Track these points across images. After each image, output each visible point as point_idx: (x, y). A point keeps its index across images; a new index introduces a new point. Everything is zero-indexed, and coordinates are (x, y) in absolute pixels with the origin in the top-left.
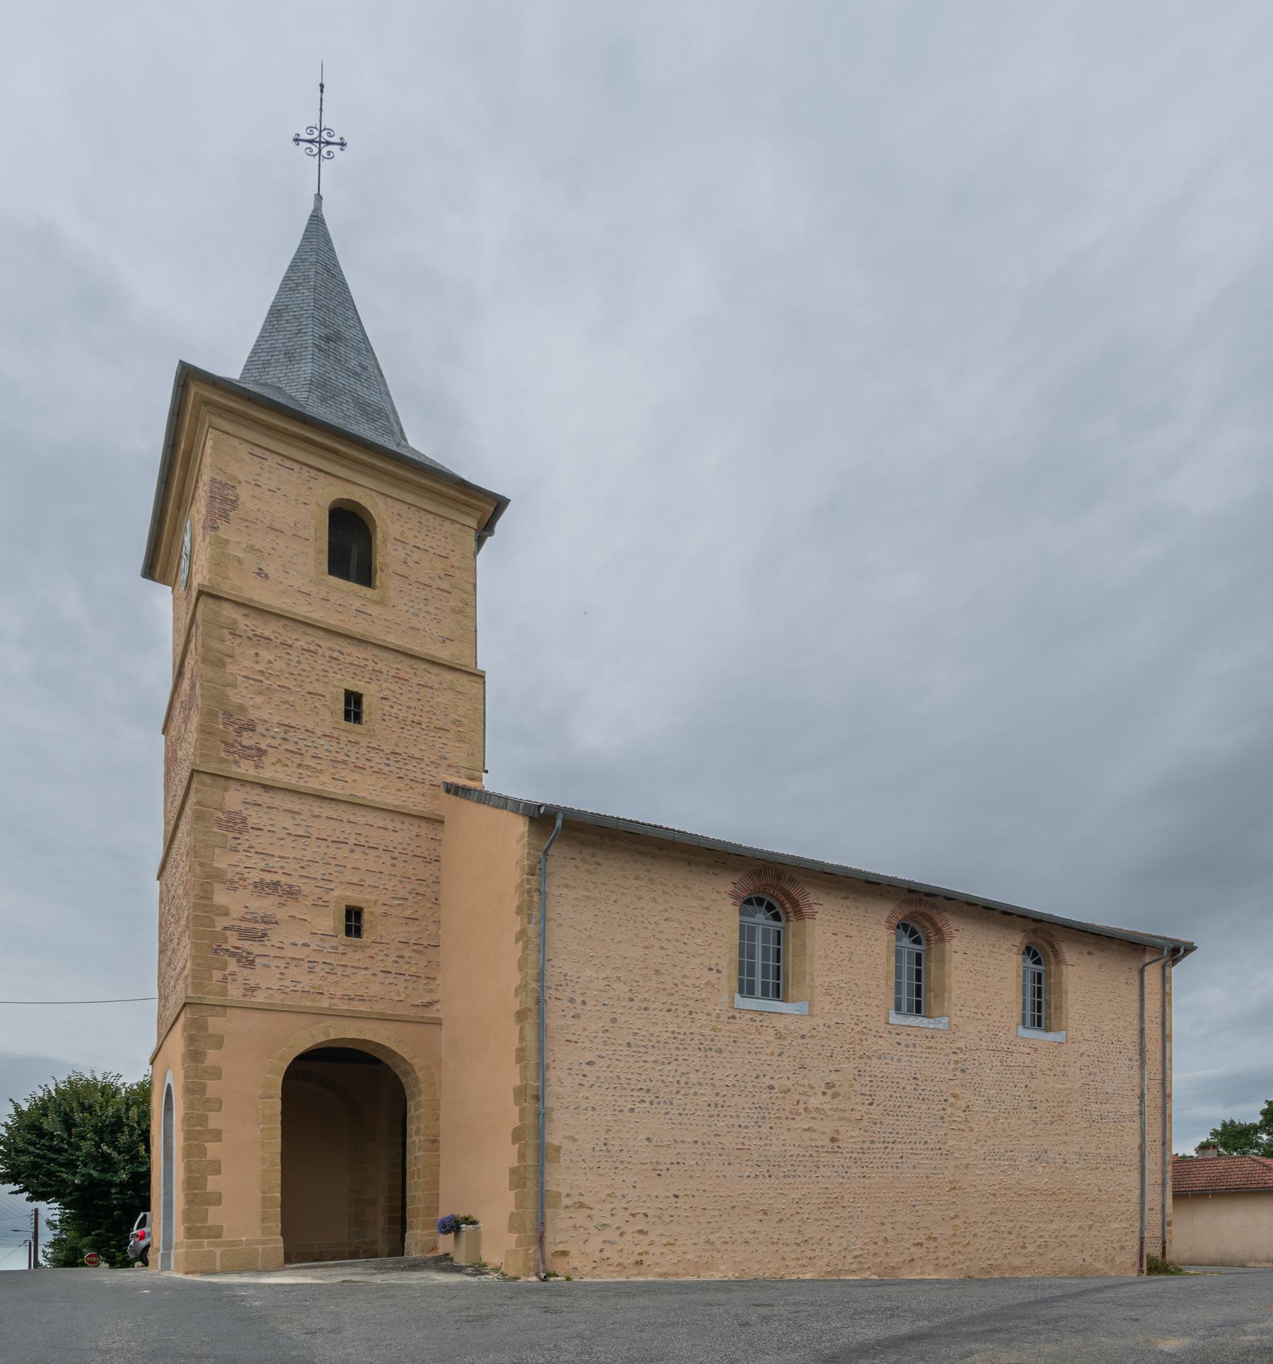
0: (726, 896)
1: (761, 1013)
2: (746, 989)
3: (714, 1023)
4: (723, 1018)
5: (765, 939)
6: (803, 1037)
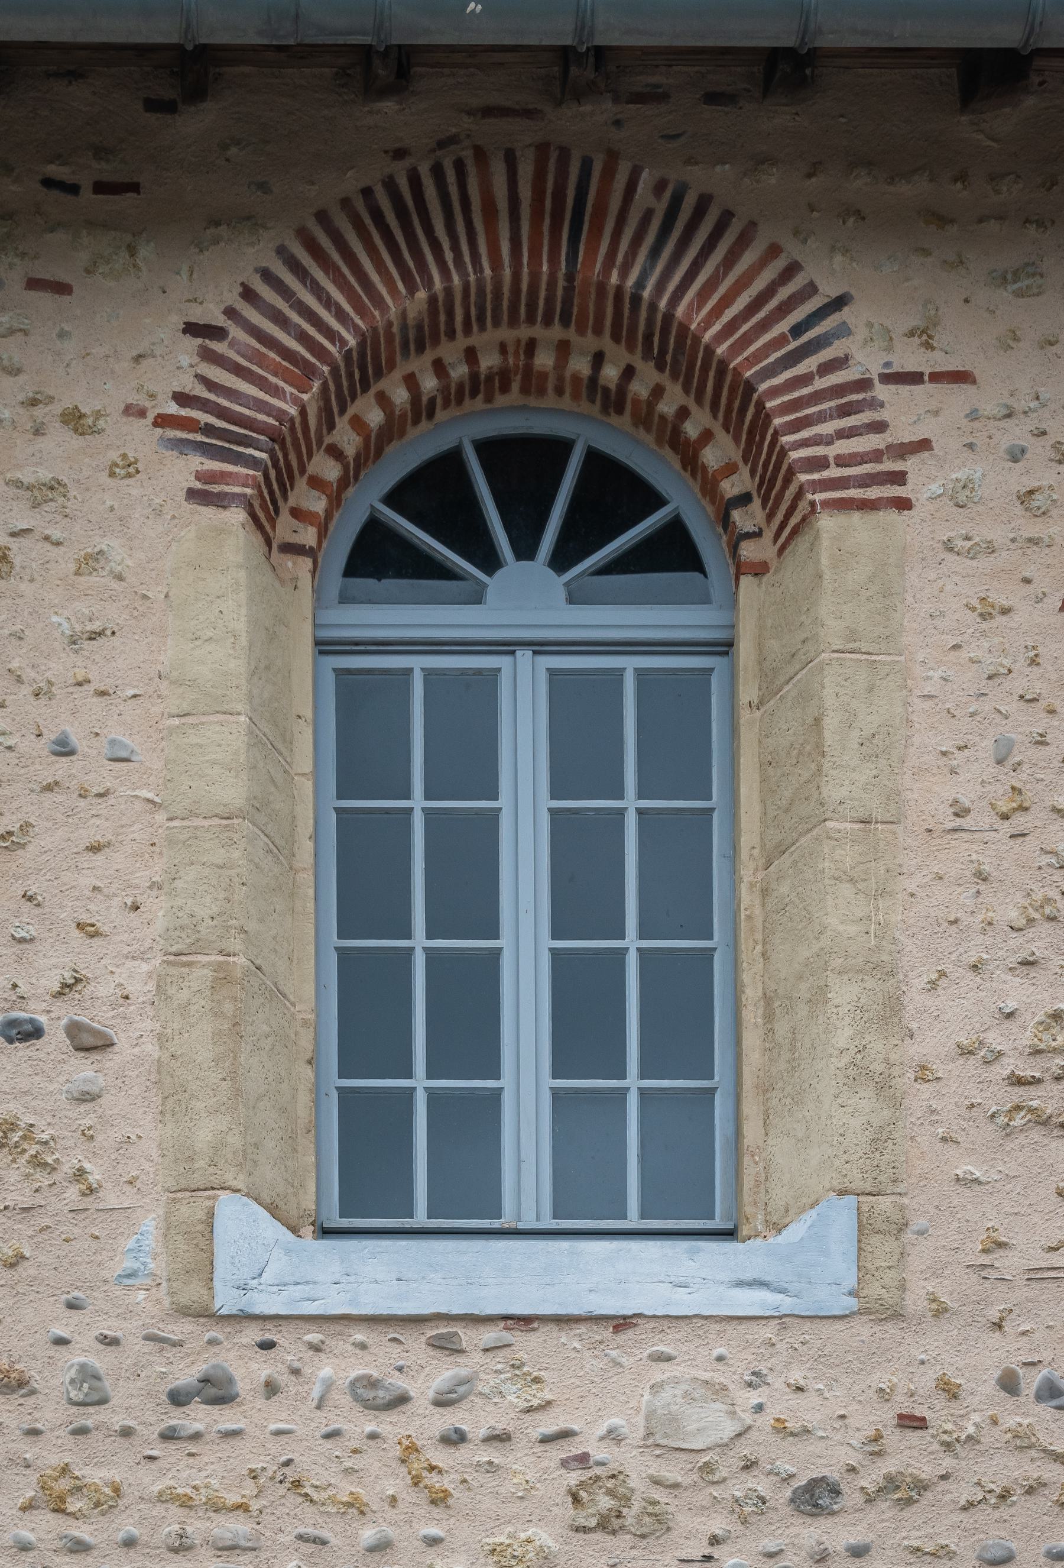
0: (141, 439)
1: (443, 1331)
2: (386, 1167)
3: (49, 1455)
4: (132, 1403)
5: (579, 758)
6: (815, 1498)
